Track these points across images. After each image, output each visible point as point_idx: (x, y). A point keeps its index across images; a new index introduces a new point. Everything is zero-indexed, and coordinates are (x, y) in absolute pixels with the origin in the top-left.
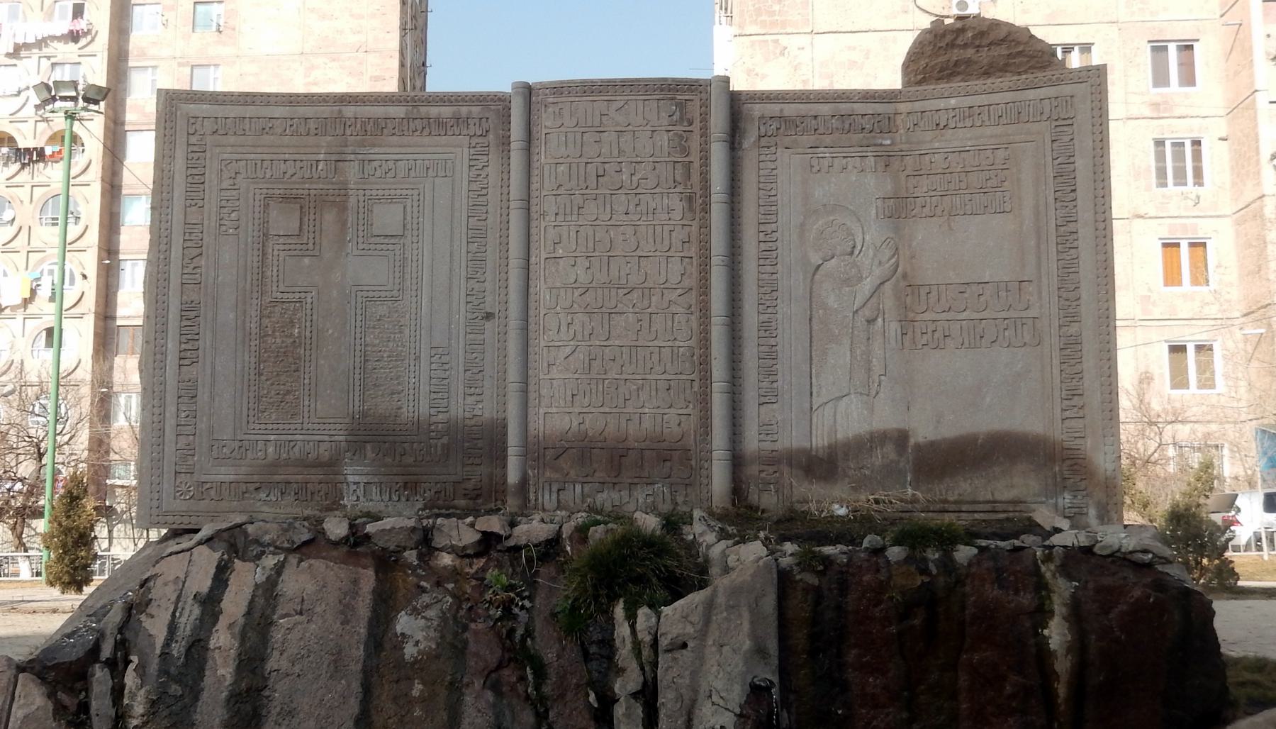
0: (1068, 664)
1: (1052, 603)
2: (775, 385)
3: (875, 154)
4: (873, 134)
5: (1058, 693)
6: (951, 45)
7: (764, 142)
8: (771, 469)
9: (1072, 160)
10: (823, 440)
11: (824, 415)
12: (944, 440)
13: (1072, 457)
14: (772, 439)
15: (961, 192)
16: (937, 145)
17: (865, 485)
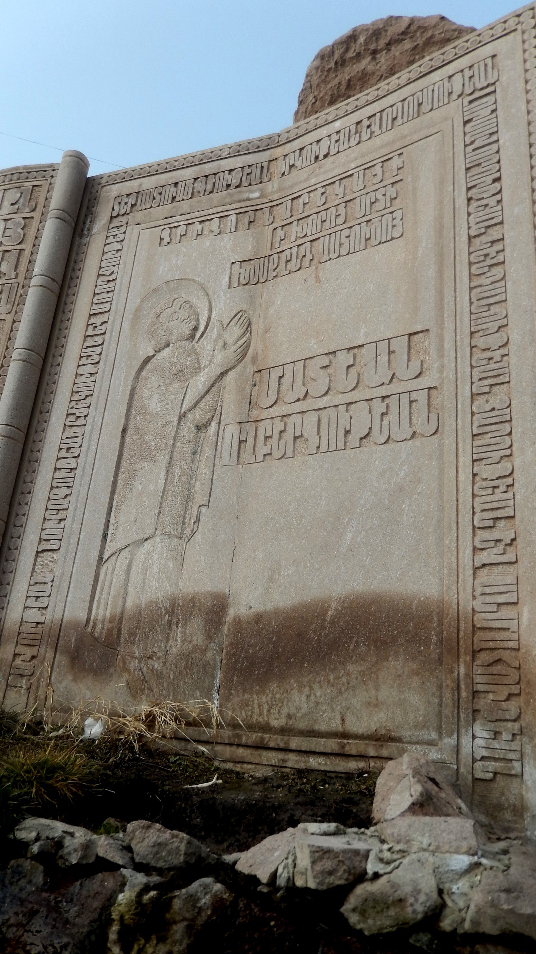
6: (342, 63)
7: (115, 223)
8: (29, 652)
11: (114, 568)
12: (276, 612)
14: (41, 605)
15: (338, 228)
16: (313, 181)
17: (150, 689)
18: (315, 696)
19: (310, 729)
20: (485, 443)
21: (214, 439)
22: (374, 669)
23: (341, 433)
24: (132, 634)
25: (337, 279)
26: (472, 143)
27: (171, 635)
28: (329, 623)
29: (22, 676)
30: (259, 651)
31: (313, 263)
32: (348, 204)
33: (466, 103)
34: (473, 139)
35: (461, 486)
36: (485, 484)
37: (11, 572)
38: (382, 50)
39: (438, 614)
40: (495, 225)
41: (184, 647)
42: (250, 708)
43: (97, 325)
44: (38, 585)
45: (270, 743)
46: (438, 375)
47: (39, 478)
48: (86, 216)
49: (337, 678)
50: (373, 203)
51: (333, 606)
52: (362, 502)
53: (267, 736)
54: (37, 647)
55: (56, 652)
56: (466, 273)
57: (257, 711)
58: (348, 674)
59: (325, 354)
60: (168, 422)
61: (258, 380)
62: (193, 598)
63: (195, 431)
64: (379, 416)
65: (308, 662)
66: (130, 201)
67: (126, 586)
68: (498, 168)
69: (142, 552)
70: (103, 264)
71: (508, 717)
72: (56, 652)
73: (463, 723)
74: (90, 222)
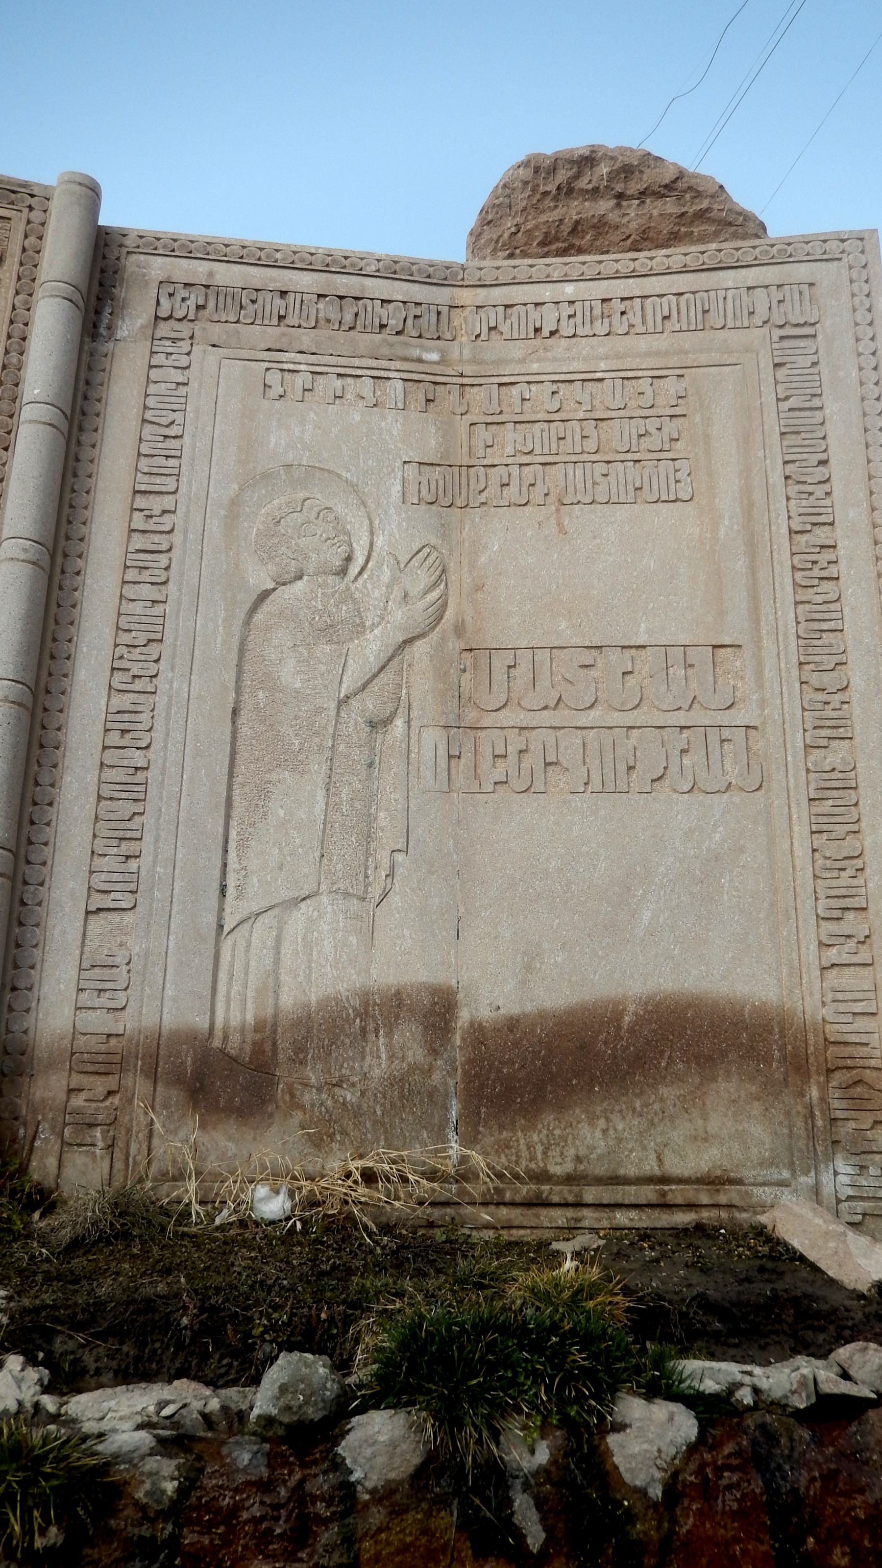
2: (133, 865)
4: (401, 338)
6: (567, 191)
7: (164, 329)
8: (100, 1085)
9: (816, 402)
11: (249, 945)
12: (542, 1015)
15: (585, 457)
16: (535, 367)
17: (344, 1132)
18: (616, 1130)
19: (613, 1175)
20: (826, 812)
21: (403, 746)
22: (699, 1093)
23: (622, 768)
24: (300, 1049)
25: (595, 537)
26: (787, 398)
27: (368, 1049)
29: (91, 1125)
30: (520, 1069)
32: (602, 424)
33: (775, 338)
35: (798, 862)
36: (828, 863)
37: (36, 946)
38: (631, 197)
39: (779, 1023)
40: (824, 524)
41: (393, 1066)
42: (514, 1151)
43: (154, 513)
44: (97, 970)
45: (551, 1197)
46: (759, 712)
47: (67, 778)
49: (646, 1105)
51: (631, 1008)
52: (662, 869)
53: (546, 1188)
54: (117, 1077)
55: (155, 1082)
56: (789, 580)
57: (525, 1154)
58: (662, 1100)
59: (587, 647)
60: (319, 710)
61: (468, 664)
62: (398, 993)
63: (368, 729)
64: (677, 752)
65: (600, 1084)
67: (276, 973)
68: (824, 447)
69: (299, 918)
70: (151, 402)
71: (875, 1149)
72: (155, 1082)
73: (821, 1158)
74: (111, 314)
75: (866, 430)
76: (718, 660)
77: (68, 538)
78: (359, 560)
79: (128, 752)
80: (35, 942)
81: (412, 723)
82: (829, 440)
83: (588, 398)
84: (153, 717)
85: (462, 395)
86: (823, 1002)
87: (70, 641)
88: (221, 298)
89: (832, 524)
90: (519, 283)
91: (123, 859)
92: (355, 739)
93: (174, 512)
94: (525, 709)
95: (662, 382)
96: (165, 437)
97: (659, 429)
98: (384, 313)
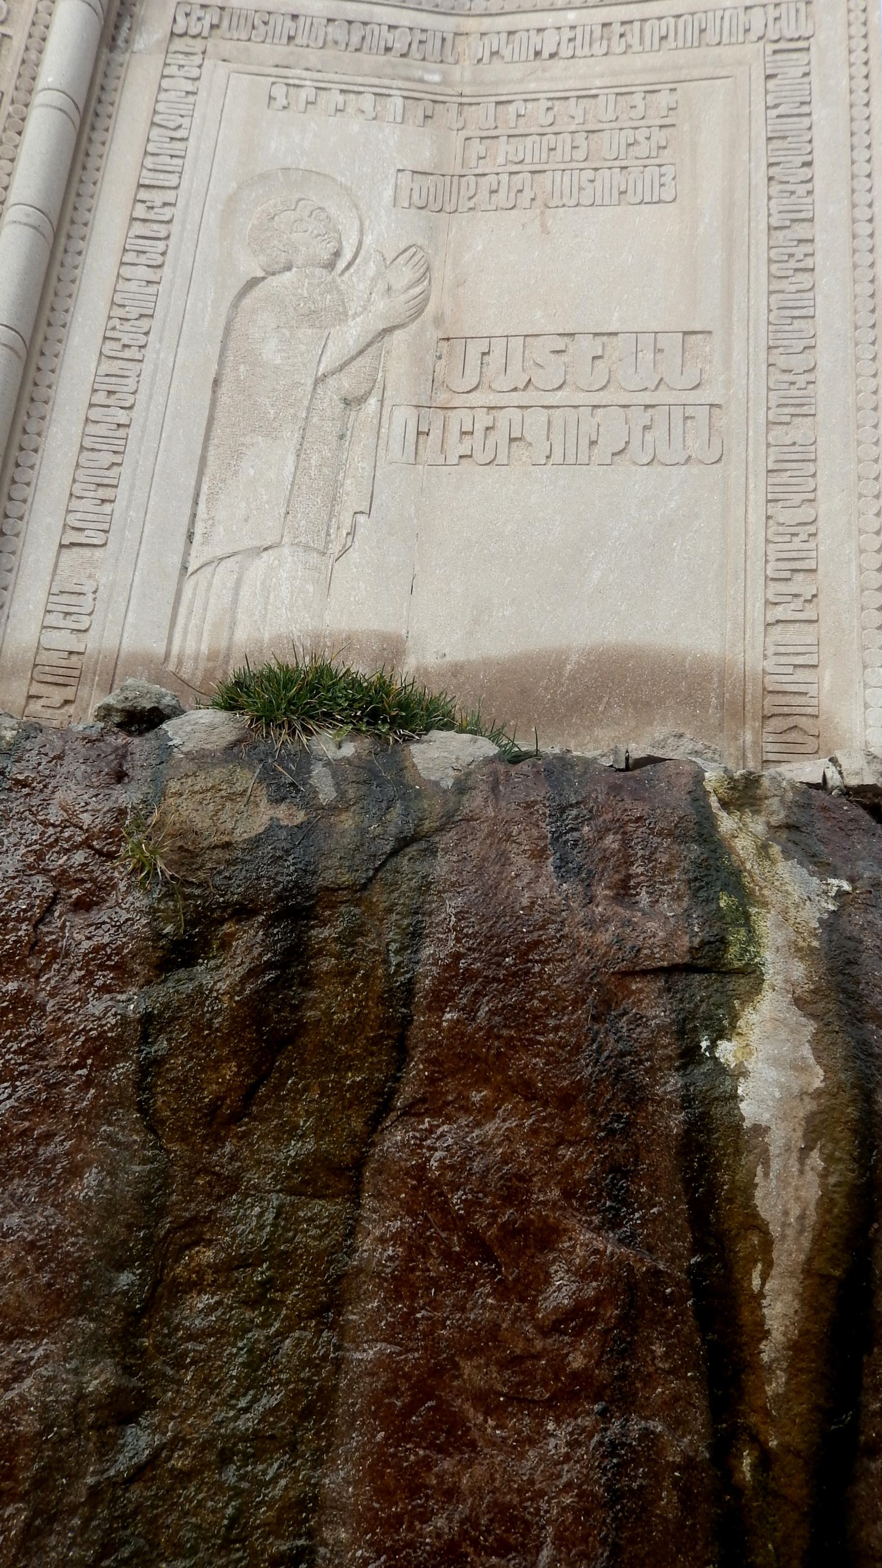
0: (812, 1193)
1: (752, 938)
2: (107, 508)
3: (406, 94)
4: (405, 60)
5: (760, 1322)
7: (179, 44)
8: (57, 695)
9: (805, 109)
10: (199, 640)
11: (210, 585)
12: (487, 663)
13: (786, 710)
15: (574, 165)
16: (532, 86)
21: (375, 421)
22: (633, 735)
23: (584, 443)
25: (576, 236)
26: (776, 106)
28: (568, 678)
31: (535, 203)
32: (591, 136)
33: (769, 51)
34: (777, 101)
35: (751, 528)
36: (781, 529)
37: (10, 571)
40: (804, 220)
43: (155, 204)
47: (53, 429)
48: (119, 15)
50: (630, 145)
52: (616, 533)
54: (74, 688)
56: (764, 271)
60: (297, 385)
61: (445, 351)
62: (349, 638)
63: (342, 406)
64: (640, 428)
66: (208, 17)
68: (809, 150)
69: (258, 567)
70: (160, 107)
74: (130, 29)
75: (852, 134)
76: (688, 346)
77: (73, 222)
78: (347, 255)
79: (112, 411)
80: (9, 567)
81: (385, 402)
82: (815, 143)
83: (581, 112)
84: (138, 382)
85: (460, 113)
86: (765, 655)
87: (67, 311)
88: (235, 19)
89: (811, 220)
90: (524, 12)
91: (99, 502)
92: (329, 412)
93: (174, 205)
94: (494, 391)
95: (654, 96)
96: (172, 139)
97: (648, 139)
98: (390, 37)
